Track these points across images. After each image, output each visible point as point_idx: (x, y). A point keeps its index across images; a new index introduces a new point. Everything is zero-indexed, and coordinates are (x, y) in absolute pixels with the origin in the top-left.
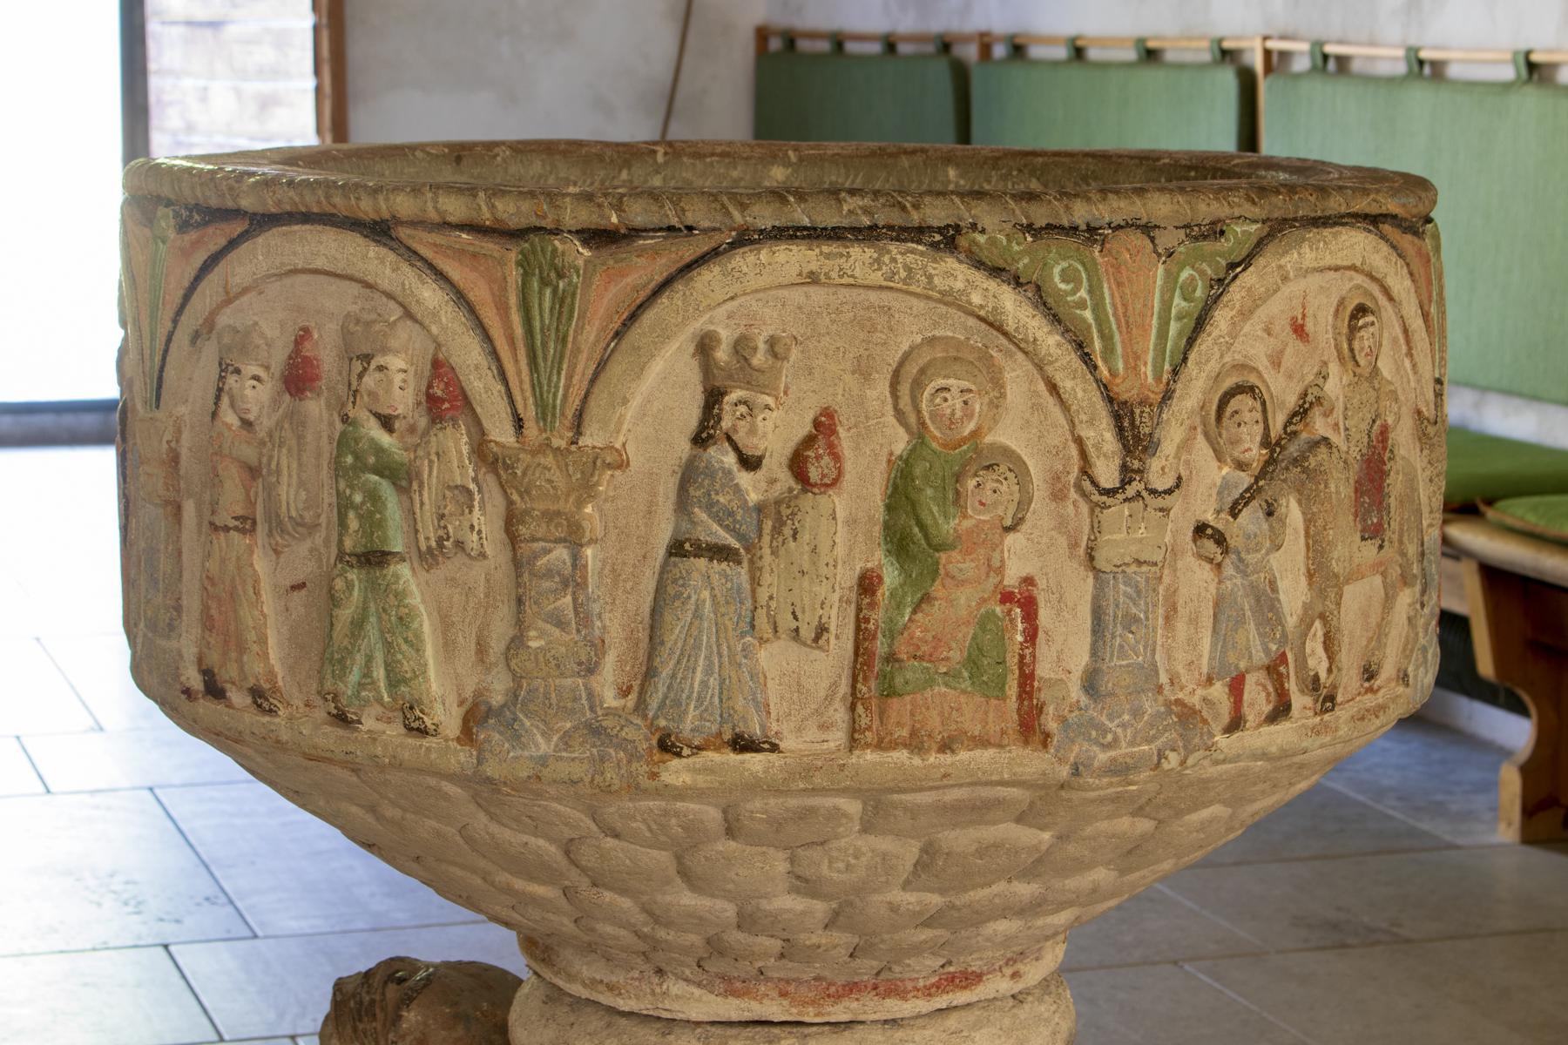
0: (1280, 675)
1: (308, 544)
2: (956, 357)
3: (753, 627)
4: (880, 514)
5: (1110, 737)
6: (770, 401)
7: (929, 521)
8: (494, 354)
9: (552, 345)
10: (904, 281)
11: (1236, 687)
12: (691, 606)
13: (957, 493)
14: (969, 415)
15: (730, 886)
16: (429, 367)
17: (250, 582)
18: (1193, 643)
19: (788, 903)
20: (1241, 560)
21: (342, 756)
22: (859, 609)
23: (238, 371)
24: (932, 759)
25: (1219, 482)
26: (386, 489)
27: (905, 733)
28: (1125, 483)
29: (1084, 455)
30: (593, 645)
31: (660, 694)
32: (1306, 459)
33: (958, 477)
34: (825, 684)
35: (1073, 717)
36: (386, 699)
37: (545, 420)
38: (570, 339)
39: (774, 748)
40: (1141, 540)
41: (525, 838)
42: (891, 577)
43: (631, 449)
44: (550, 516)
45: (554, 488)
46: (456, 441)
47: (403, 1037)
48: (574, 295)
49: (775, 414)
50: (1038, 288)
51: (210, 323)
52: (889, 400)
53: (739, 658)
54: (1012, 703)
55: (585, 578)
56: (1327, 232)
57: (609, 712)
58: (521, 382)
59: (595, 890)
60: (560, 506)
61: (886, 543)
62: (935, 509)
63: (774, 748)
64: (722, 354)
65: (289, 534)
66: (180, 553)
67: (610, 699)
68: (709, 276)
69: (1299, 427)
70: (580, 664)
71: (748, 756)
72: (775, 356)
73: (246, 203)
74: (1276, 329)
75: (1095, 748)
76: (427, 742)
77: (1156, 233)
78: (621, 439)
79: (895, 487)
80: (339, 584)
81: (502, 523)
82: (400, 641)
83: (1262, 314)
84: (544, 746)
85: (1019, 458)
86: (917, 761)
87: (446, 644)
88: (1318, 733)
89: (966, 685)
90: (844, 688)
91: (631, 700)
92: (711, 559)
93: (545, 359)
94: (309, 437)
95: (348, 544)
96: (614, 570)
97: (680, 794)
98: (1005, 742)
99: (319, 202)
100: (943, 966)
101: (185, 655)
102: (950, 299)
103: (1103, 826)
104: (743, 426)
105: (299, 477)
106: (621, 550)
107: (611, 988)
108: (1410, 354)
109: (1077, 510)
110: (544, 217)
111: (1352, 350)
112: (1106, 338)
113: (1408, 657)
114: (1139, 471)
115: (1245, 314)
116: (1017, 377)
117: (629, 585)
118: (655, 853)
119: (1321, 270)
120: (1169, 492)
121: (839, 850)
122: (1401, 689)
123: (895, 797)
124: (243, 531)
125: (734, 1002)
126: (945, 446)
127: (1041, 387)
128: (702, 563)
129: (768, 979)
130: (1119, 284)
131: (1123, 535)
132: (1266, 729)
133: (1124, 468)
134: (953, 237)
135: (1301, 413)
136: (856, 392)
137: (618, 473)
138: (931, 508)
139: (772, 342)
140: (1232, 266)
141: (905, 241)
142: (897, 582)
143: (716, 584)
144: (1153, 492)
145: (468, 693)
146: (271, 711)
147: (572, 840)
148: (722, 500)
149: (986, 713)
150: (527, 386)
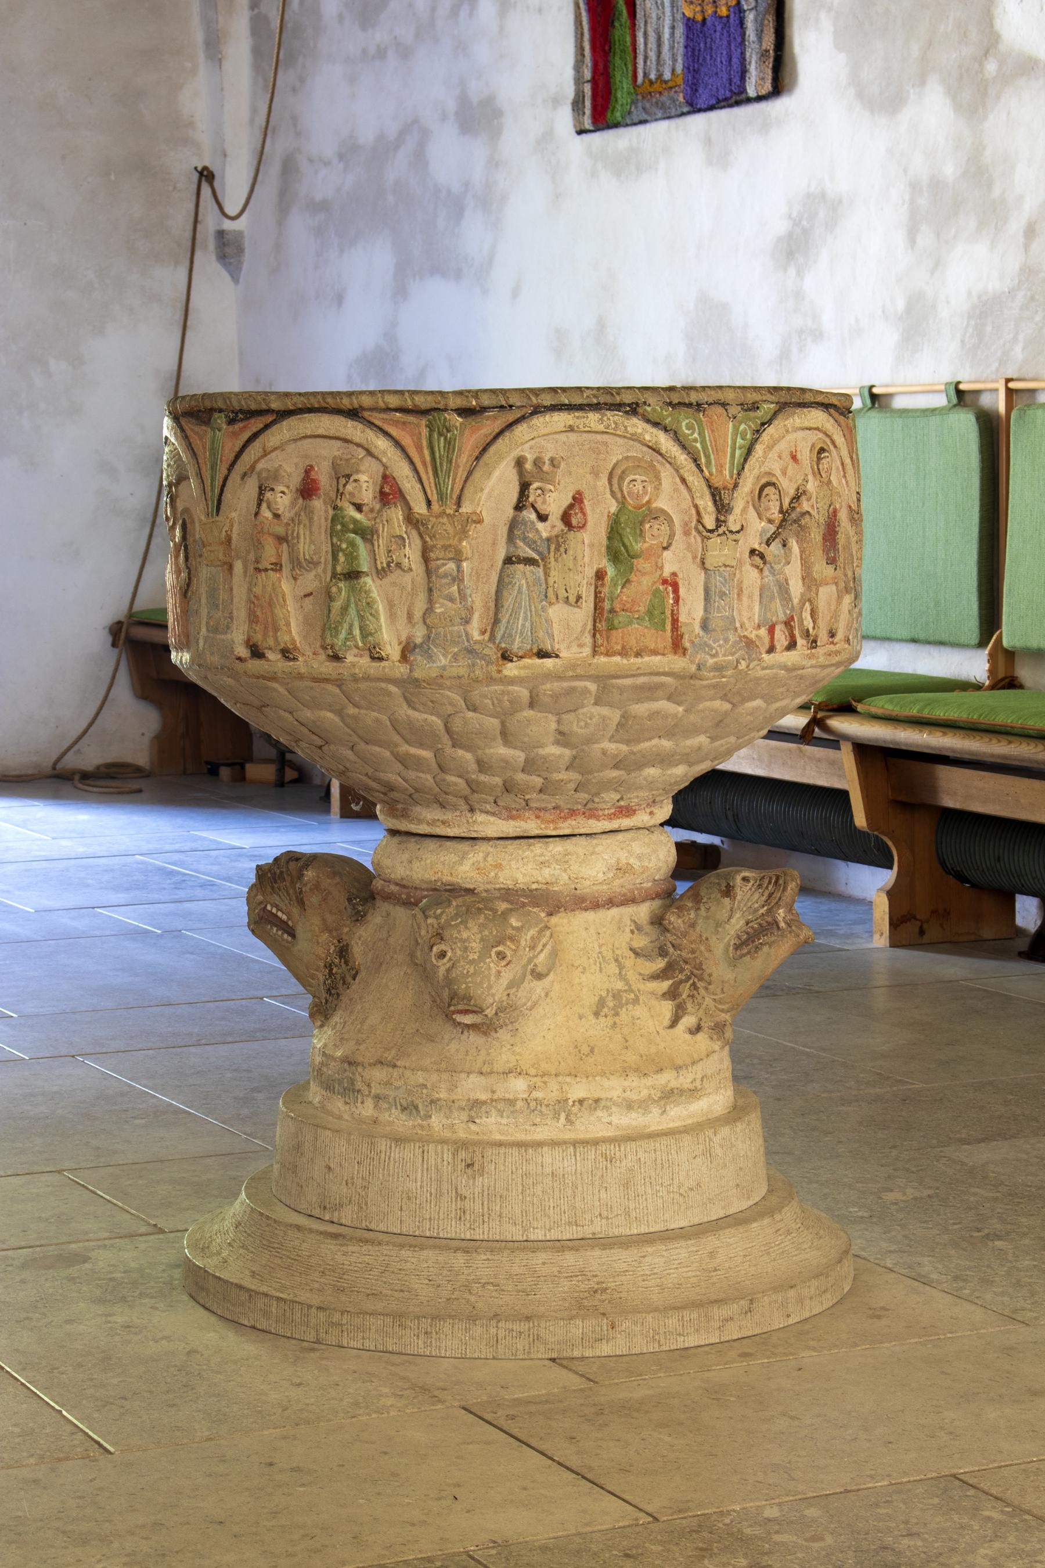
0: (791, 626)
1: (313, 573)
2: (638, 465)
3: (546, 597)
4: (605, 542)
5: (714, 651)
6: (552, 488)
7: (628, 544)
8: (416, 470)
9: (445, 464)
10: (614, 429)
11: (771, 630)
12: (516, 588)
13: (641, 530)
14: (646, 493)
15: (526, 739)
16: (380, 479)
17: (280, 596)
18: (750, 608)
19: (553, 750)
20: (772, 567)
21: (336, 677)
22: (596, 587)
23: (272, 490)
24: (632, 660)
25: (760, 529)
26: (358, 540)
27: (619, 647)
28: (718, 527)
29: (698, 513)
30: (468, 609)
31: (502, 632)
32: (800, 520)
33: (642, 523)
34: (581, 624)
35: (697, 641)
36: (360, 644)
37: (442, 501)
38: (454, 461)
39: (557, 656)
40: (726, 555)
41: (426, 716)
42: (611, 571)
43: (484, 514)
44: (446, 548)
45: (448, 533)
46: (397, 514)
47: (305, 885)
48: (455, 440)
49: (554, 494)
50: (675, 433)
51: (253, 468)
52: (608, 486)
53: (540, 612)
54: (669, 633)
55: (463, 577)
56: (805, 410)
57: (476, 642)
58: (430, 483)
59: (454, 749)
60: (451, 542)
61: (608, 555)
62: (631, 538)
63: (557, 656)
64: (528, 466)
65: (304, 568)
66: (231, 589)
67: (476, 636)
68: (521, 429)
69: (796, 505)
70: (462, 619)
71: (545, 660)
72: (554, 466)
73: (274, 406)
74: (784, 456)
75: (707, 656)
76: (384, 664)
77: (728, 407)
78: (480, 509)
79: (612, 528)
80: (334, 590)
81: (420, 554)
82: (368, 614)
83: (777, 448)
84: (443, 661)
85: (668, 514)
86: (625, 661)
87: (391, 615)
88: (810, 658)
89: (647, 624)
90: (590, 626)
91: (487, 636)
92: (525, 565)
93: (442, 471)
94: (316, 518)
95: (339, 569)
96: (477, 573)
97: (512, 681)
98: (666, 652)
99: (319, 402)
100: (618, 801)
101: (236, 641)
102: (635, 438)
103: (708, 704)
104: (540, 500)
105: (310, 538)
106: (481, 562)
107: (444, 822)
108: (845, 476)
109: (695, 540)
110: (439, 403)
111: (819, 469)
112: (707, 457)
113: (850, 630)
114: (724, 522)
115: (770, 447)
116: (667, 475)
117: (484, 580)
118: (492, 720)
119: (803, 429)
120: (738, 532)
121: (583, 714)
122: (847, 646)
123: (614, 681)
124: (275, 570)
125: (512, 823)
126: (635, 508)
127: (678, 480)
128: (521, 566)
129: (531, 809)
130: (713, 431)
131: (718, 552)
132: (785, 653)
133: (717, 520)
134: (635, 409)
135: (797, 498)
136: (592, 483)
137: (478, 525)
138: (629, 539)
139: (552, 460)
140: (763, 424)
141: (613, 410)
142: (614, 574)
143: (528, 576)
144: (731, 532)
145: (403, 639)
146: (294, 659)
147: (449, 715)
148: (530, 535)
149: (657, 638)
150: (433, 485)
